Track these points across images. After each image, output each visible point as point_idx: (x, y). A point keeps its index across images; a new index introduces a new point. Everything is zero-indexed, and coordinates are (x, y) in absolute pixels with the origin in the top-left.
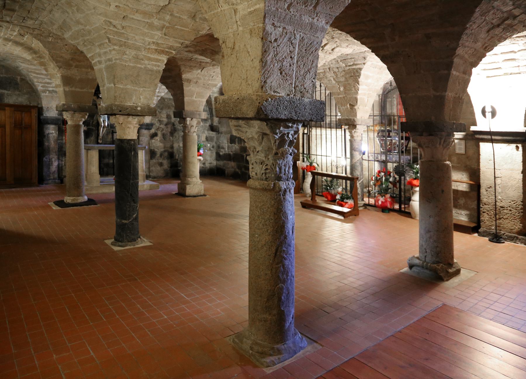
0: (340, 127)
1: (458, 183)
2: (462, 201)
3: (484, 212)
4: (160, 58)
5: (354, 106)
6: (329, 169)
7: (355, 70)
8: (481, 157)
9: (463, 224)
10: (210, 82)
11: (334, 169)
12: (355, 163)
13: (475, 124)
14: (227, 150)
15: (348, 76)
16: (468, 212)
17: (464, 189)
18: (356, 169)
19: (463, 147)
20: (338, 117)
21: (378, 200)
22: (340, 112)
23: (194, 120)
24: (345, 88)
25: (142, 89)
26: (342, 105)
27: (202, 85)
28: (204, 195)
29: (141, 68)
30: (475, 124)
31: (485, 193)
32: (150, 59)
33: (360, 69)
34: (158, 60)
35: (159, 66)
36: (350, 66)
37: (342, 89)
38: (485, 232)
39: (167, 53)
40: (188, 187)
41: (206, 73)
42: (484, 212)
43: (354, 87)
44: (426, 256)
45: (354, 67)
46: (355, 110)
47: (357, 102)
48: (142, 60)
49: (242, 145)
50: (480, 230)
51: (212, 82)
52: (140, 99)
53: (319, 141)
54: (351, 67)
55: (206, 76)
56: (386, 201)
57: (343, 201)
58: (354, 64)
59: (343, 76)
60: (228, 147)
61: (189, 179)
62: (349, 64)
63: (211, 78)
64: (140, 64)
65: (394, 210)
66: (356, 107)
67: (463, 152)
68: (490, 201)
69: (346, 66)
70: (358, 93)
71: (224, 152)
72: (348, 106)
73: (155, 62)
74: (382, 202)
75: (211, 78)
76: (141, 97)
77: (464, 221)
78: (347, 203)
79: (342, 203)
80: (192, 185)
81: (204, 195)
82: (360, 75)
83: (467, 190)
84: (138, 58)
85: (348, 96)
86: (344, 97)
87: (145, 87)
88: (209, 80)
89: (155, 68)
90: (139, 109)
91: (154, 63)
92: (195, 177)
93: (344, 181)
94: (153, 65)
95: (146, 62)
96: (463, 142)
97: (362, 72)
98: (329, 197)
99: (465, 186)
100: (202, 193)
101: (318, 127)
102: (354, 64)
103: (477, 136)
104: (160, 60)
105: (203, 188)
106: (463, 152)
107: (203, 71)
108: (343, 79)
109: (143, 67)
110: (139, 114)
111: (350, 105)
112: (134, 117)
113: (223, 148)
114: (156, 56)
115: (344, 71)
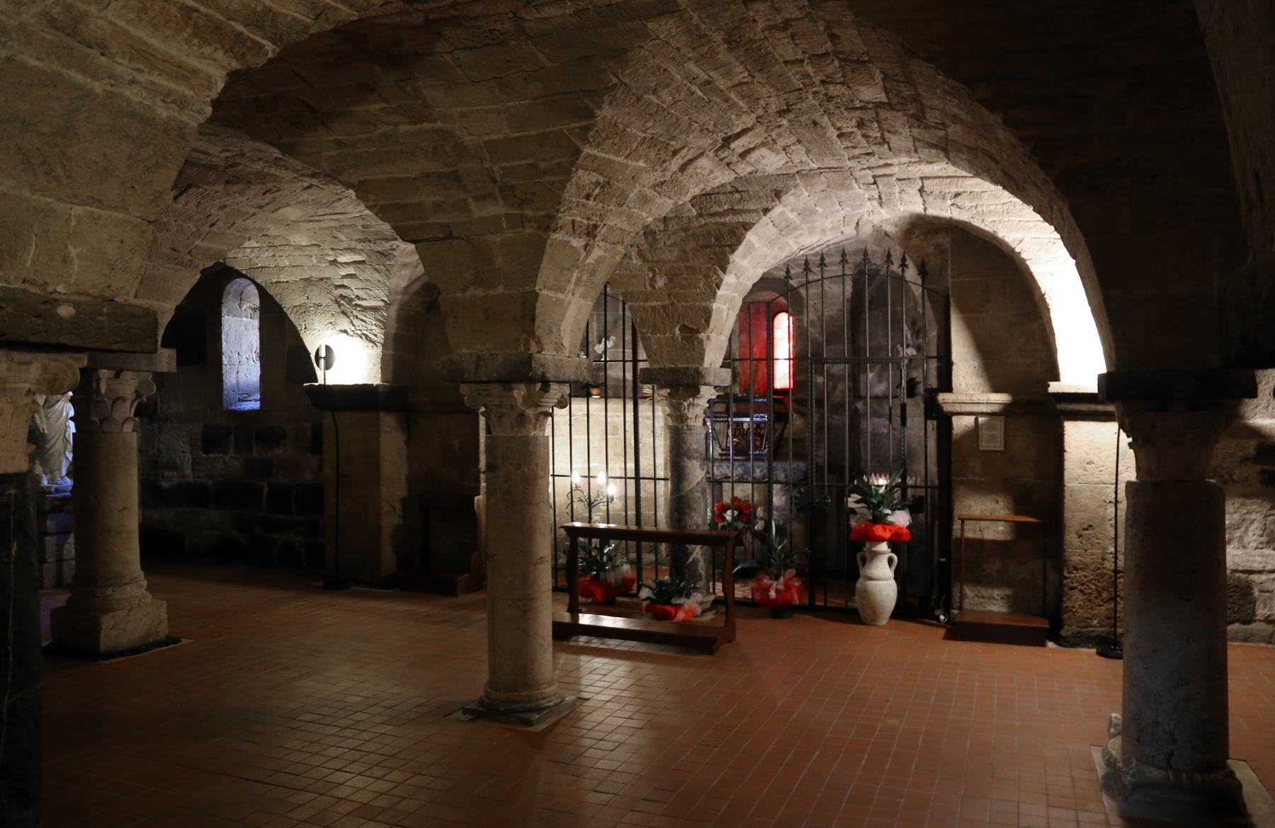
0: (584, 392)
1: (983, 524)
2: (993, 567)
3: (1072, 589)
4: (195, 63)
5: (697, 331)
6: (580, 508)
7: (726, 229)
8: (1066, 455)
9: (998, 621)
10: (198, 242)
11: (580, 508)
12: (690, 491)
13: (1057, 378)
14: (188, 471)
15: (693, 244)
16: (1008, 592)
17: (1000, 537)
18: (695, 510)
19: (999, 433)
20: (642, 365)
21: (767, 590)
22: (646, 349)
23: (128, 375)
24: (671, 280)
25: (78, 210)
26: (655, 329)
27: (166, 250)
28: (171, 640)
29: (88, 94)
30: (1057, 378)
31: (1076, 542)
32: (141, 54)
33: (747, 227)
34: (185, 74)
35: (182, 103)
36: (714, 215)
37: (661, 282)
38: (1074, 636)
39: (235, 44)
40: (107, 621)
41: (192, 206)
42: (1072, 589)
43: (707, 276)
44: (1171, 754)
45: (728, 219)
46: (701, 342)
47: (708, 321)
48: (104, 49)
49: (255, 454)
50: (1063, 633)
51: (206, 244)
52: (66, 260)
53: (579, 438)
54: (717, 219)
55: (190, 219)
56: (788, 587)
57: (668, 602)
58: (726, 213)
59: (675, 244)
60: (195, 463)
61: (110, 591)
62: (716, 209)
63: (205, 228)
64: (84, 71)
65: (801, 609)
66: (702, 336)
67: (999, 446)
68: (1088, 560)
69: (700, 215)
70: (715, 293)
71: (176, 480)
72: (677, 332)
73: (170, 76)
74: (777, 591)
75: (205, 228)
76: (73, 251)
77: (1000, 613)
78: (681, 605)
79: (668, 608)
80: (122, 613)
81: (176, 641)
82: (739, 242)
83: (1009, 538)
84: (73, 34)
85: (679, 305)
86: (664, 307)
87: (99, 203)
88: (197, 234)
89: (163, 112)
90: (65, 311)
91: (162, 81)
92: (134, 580)
93: (632, 544)
94: (154, 90)
95: (122, 67)
96: (1000, 422)
97: (750, 236)
98: (599, 594)
99: (1001, 528)
100: (163, 631)
101: (616, 397)
102: (733, 211)
103: (1063, 406)
104: (195, 72)
105: (164, 615)
106: (999, 446)
107: (183, 199)
108: (671, 255)
109: (97, 87)
110: (65, 339)
111: (684, 329)
112: (18, 356)
113: (172, 466)
114: (175, 48)
115: (685, 230)
